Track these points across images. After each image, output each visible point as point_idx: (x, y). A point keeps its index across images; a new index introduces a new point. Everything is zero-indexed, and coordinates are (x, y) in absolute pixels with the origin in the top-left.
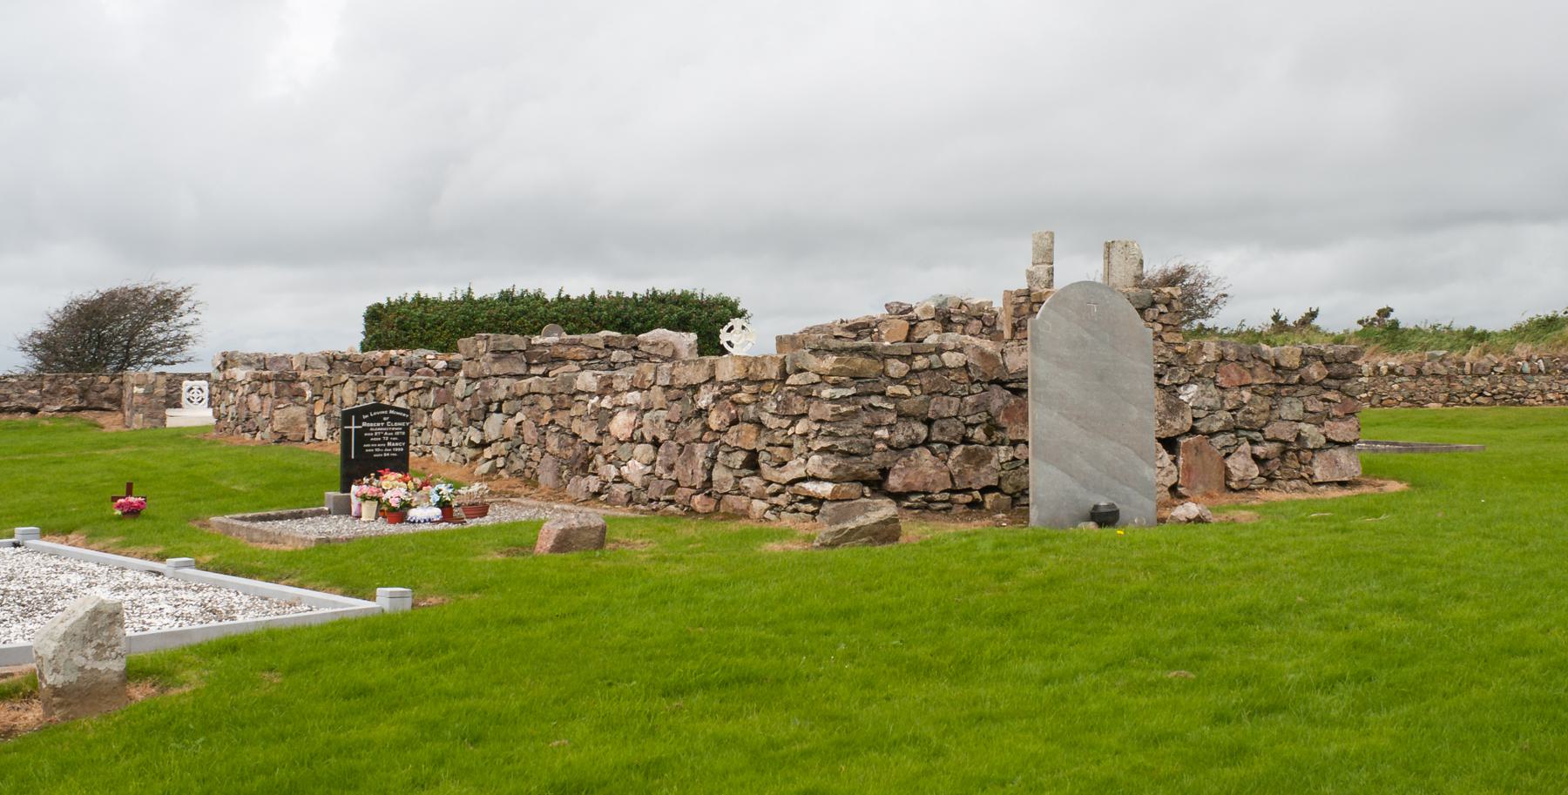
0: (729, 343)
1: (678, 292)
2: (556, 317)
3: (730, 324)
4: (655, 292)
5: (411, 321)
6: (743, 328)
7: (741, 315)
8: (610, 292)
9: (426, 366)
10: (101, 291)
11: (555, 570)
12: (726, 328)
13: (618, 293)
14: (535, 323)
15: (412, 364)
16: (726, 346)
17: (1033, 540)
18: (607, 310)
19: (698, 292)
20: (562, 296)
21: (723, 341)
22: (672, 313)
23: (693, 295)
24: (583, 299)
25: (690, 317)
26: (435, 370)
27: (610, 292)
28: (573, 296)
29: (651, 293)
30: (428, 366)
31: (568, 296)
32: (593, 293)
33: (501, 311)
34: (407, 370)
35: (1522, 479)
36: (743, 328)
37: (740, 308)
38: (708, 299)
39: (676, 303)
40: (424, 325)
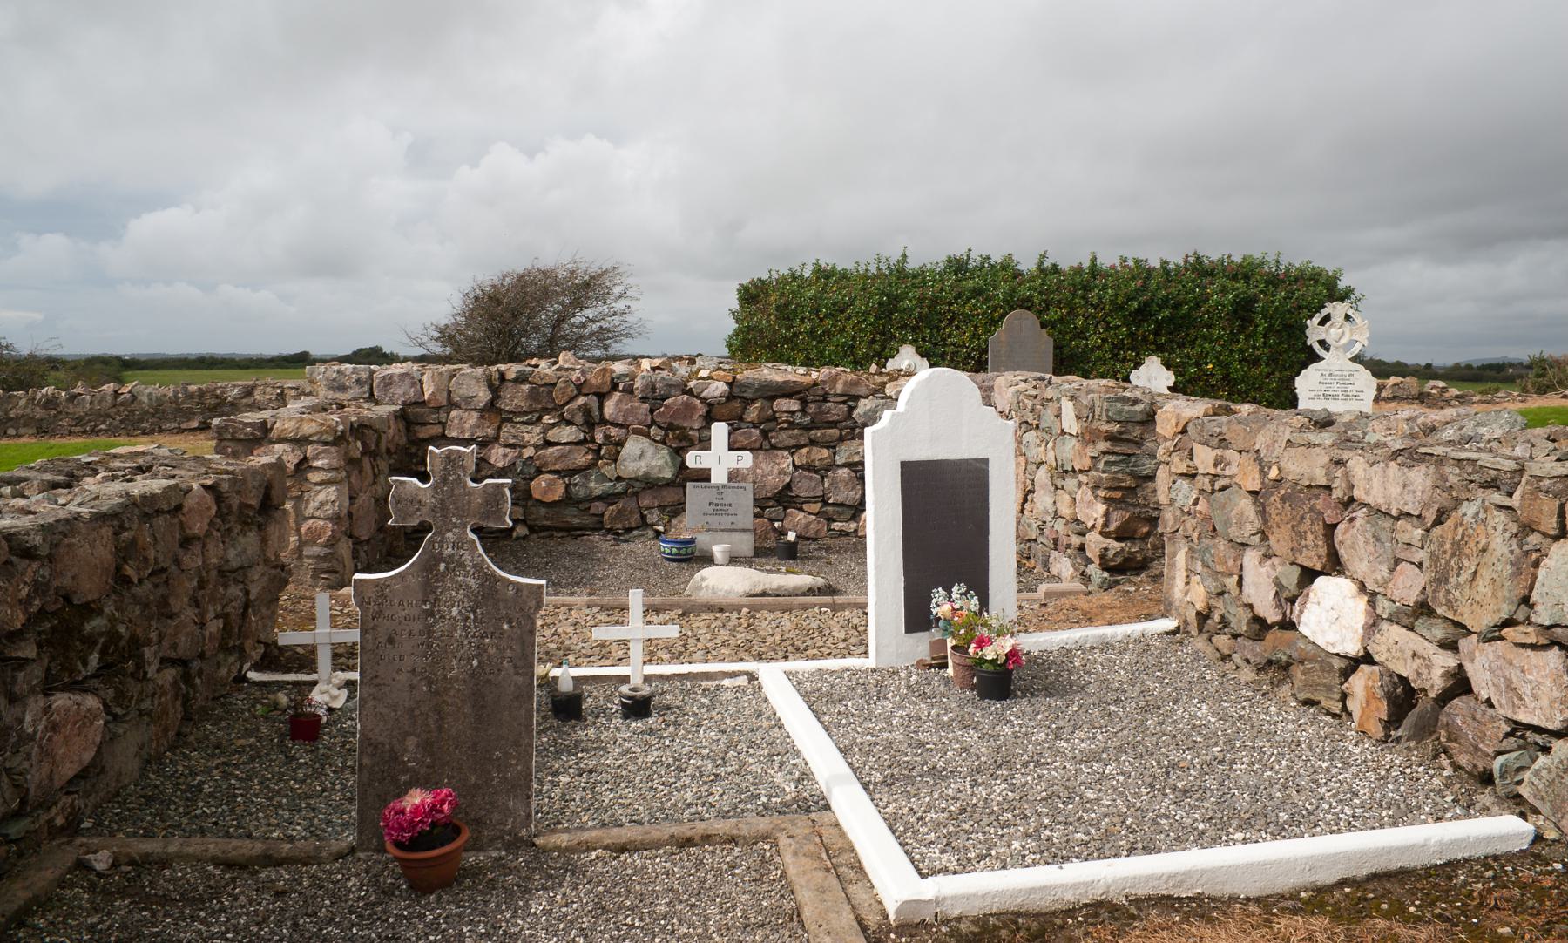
0: (1322, 343)
1: (1237, 259)
2: (1029, 299)
3: (1324, 312)
4: (1198, 259)
5: (798, 305)
6: (1348, 317)
7: (1345, 296)
8: (1124, 260)
9: (685, 392)
10: (1232, 258)
11: (980, 781)
12: (1317, 319)
13: (1137, 262)
14: (995, 309)
15: (654, 389)
16: (1316, 347)
17: (102, 891)
18: (1116, 288)
19: (1271, 258)
20: (1047, 264)
21: (1312, 341)
22: (1224, 291)
23: (1262, 263)
24: (1078, 271)
25: (1255, 299)
26: (704, 400)
27: (1124, 260)
28: (1065, 265)
29: (1191, 260)
30: (690, 392)
31: (1055, 266)
32: (1094, 260)
33: (942, 290)
34: (644, 399)
35: (931, 666)
36: (1348, 317)
37: (1342, 284)
38: (1288, 270)
39: (1235, 278)
40: (818, 311)
